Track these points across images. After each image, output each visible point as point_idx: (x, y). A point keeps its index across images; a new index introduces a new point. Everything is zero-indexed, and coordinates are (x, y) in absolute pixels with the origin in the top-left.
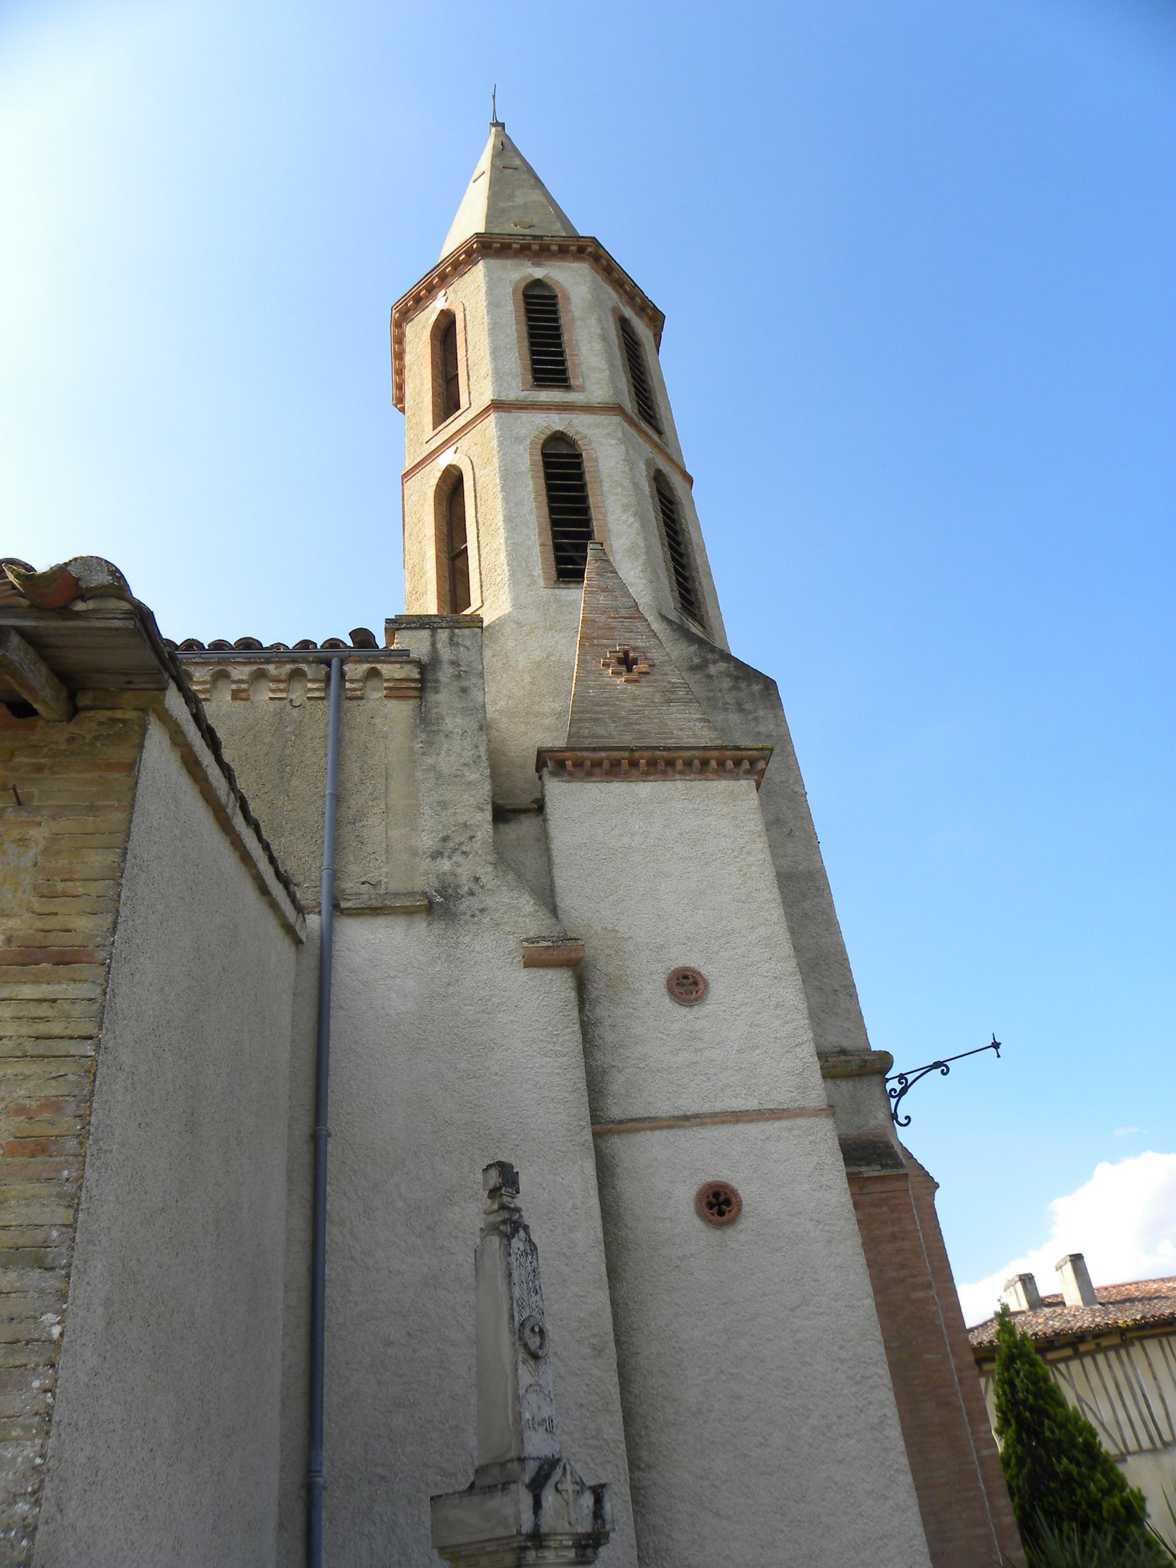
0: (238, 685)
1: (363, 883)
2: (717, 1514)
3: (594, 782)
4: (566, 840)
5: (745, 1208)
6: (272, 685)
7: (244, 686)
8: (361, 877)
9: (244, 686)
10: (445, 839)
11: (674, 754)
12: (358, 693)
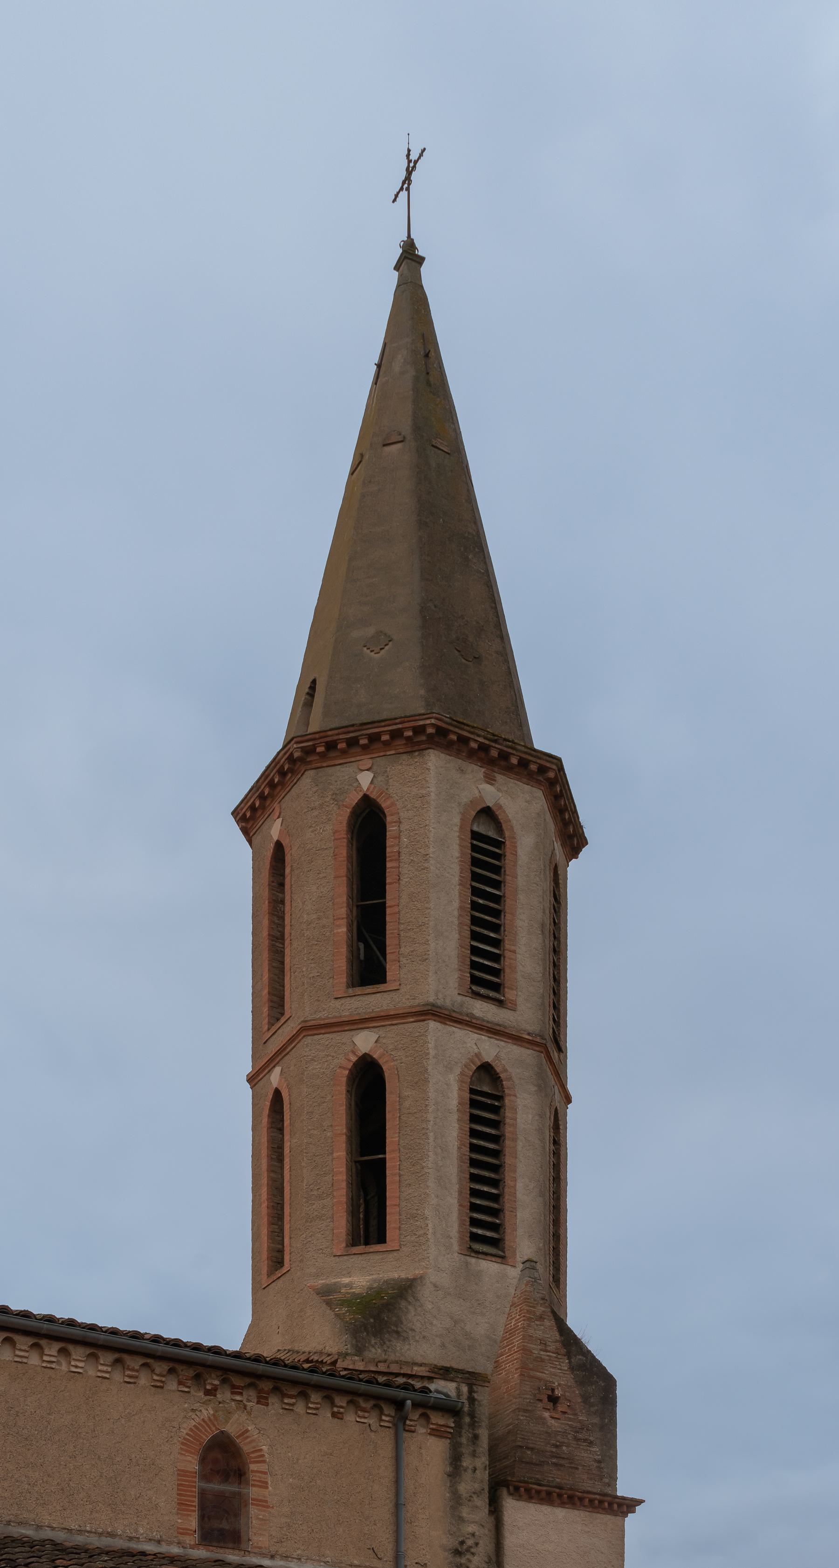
0: (339, 1409)
1: (416, 1563)
3: (533, 1503)
4: (513, 1540)
7: (342, 1410)
8: (415, 1559)
9: (342, 1410)
10: (462, 1543)
11: (585, 1495)
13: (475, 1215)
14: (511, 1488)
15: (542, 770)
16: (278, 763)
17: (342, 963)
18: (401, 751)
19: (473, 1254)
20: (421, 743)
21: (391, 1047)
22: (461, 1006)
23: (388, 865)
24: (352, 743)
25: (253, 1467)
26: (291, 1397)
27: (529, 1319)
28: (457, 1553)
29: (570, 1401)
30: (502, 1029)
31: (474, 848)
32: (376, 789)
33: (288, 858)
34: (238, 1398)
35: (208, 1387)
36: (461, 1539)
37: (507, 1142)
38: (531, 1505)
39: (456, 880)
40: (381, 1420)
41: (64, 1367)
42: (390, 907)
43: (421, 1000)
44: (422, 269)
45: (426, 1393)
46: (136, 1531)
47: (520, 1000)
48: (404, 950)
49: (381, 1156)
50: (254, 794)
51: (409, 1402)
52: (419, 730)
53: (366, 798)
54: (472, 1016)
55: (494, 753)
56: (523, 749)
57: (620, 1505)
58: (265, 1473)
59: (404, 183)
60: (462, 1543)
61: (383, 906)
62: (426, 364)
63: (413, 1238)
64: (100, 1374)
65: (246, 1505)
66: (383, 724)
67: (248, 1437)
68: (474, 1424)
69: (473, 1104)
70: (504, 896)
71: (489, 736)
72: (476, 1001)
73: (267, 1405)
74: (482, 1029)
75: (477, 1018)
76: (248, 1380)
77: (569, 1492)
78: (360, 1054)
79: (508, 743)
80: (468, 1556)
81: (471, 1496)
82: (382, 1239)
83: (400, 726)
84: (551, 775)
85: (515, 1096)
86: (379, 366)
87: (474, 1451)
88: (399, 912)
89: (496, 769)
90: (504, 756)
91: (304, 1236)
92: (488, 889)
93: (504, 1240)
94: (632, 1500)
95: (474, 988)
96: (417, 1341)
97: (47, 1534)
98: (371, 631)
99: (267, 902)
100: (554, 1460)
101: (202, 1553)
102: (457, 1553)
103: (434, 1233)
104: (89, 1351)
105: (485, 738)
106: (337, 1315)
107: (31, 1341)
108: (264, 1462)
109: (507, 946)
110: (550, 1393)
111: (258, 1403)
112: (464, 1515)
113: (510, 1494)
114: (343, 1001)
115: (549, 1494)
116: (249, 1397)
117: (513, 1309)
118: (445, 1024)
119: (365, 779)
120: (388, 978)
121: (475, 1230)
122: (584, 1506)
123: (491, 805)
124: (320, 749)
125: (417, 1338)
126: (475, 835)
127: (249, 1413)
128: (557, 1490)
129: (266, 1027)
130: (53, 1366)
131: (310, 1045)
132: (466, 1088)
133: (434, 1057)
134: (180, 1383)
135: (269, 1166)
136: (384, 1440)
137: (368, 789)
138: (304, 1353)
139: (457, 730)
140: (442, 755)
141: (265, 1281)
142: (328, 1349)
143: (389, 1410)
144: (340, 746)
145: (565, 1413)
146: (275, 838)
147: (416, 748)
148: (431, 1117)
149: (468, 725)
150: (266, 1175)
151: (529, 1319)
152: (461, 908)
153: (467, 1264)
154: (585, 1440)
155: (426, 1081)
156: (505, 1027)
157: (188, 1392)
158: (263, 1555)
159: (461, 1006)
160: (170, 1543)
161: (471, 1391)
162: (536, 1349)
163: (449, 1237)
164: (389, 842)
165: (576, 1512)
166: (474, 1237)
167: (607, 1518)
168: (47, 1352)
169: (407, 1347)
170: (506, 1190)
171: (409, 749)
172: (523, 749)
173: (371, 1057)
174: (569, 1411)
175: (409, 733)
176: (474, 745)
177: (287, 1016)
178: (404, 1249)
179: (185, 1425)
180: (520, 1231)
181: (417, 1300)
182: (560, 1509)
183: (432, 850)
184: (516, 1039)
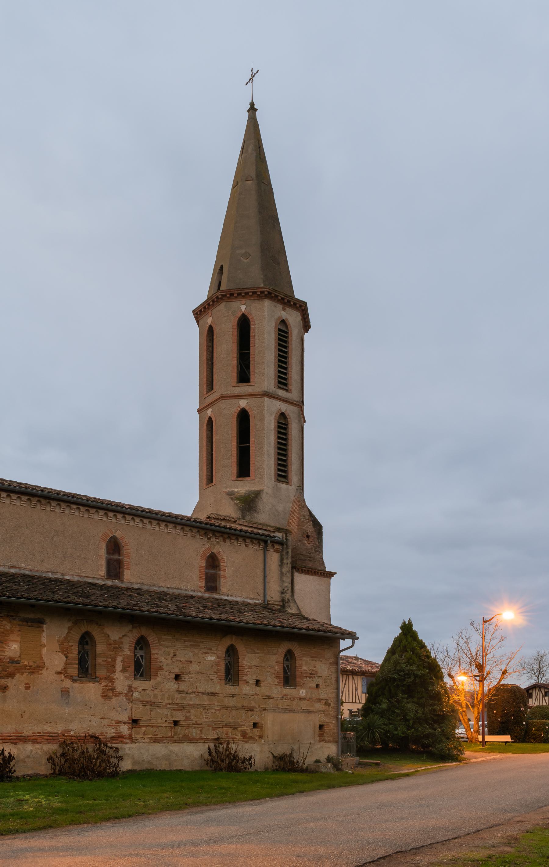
9: (248, 544)
10: (284, 589)
13: (279, 467)
14: (297, 569)
15: (301, 306)
16: (213, 297)
17: (235, 374)
18: (255, 298)
20: (262, 296)
21: (252, 406)
22: (275, 392)
23: (251, 340)
24: (239, 294)
25: (222, 564)
26: (233, 540)
27: (300, 508)
28: (282, 593)
29: (313, 537)
30: (288, 400)
31: (279, 334)
32: (247, 312)
33: (215, 333)
34: (217, 540)
35: (209, 537)
36: (283, 588)
37: (289, 441)
38: (302, 575)
39: (273, 346)
40: (260, 547)
41: (166, 531)
42: (252, 355)
43: (262, 390)
44: (256, 112)
45: (274, 538)
46: (187, 587)
47: (293, 389)
48: (257, 371)
49: (248, 445)
50: (202, 306)
51: (269, 541)
52: (262, 292)
53: (243, 314)
54: (278, 395)
55: (286, 301)
57: (329, 574)
59: (250, 80)
60: (284, 589)
61: (249, 353)
62: (259, 150)
63: (260, 476)
64: (177, 533)
65: (220, 577)
66: (250, 289)
67: (220, 554)
68: (287, 548)
69: (279, 427)
70: (288, 352)
71: (285, 295)
73: (226, 542)
74: (281, 400)
75: (280, 396)
76: (221, 534)
77: (315, 570)
78: (241, 408)
80: (286, 594)
82: (248, 475)
83: (256, 290)
84: (303, 308)
85: (292, 424)
86: (243, 149)
87: (287, 557)
88: (255, 357)
89: (286, 306)
90: (289, 302)
91: (222, 473)
93: (288, 476)
94: (333, 573)
95: (279, 385)
96: (261, 513)
97: (162, 589)
98: (243, 251)
99: (206, 346)
100: (309, 559)
101: (207, 595)
102: (282, 593)
103: (267, 474)
104: (174, 525)
105: (283, 295)
106: (236, 504)
107: (157, 522)
108: (225, 562)
109: (289, 370)
110: (307, 534)
112: (284, 580)
113: (296, 571)
114: (235, 388)
115: (308, 571)
116: (220, 540)
117: (294, 503)
119: (243, 308)
120: (251, 381)
121: (279, 473)
122: (319, 575)
123: (284, 319)
124: (228, 296)
125: (261, 512)
126: (280, 330)
127: (221, 546)
128: (311, 570)
129: (205, 393)
130: (163, 530)
131: (224, 403)
132: (277, 421)
133: (267, 411)
134: (200, 535)
135: (207, 444)
136: (260, 554)
137: (244, 311)
138: (222, 516)
139: (275, 293)
140: (269, 301)
141: (205, 487)
142: (232, 516)
143: (262, 544)
144: (235, 295)
145: (311, 541)
146: (209, 323)
147: (261, 298)
148: (265, 432)
149: (278, 291)
150: (205, 447)
151: (300, 508)
152: (275, 356)
153: (277, 485)
154: (318, 551)
155: (264, 419)
156: (288, 399)
157: (202, 538)
158: (225, 595)
159: (275, 392)
160: (198, 592)
161: (286, 536)
162: (302, 518)
163: (271, 476)
164: (251, 331)
165: (316, 577)
166: (279, 475)
167: (325, 579)
168: (161, 526)
169: (258, 515)
170: (289, 458)
171: (258, 298)
173: (245, 409)
174: (313, 541)
175: (259, 293)
176: (280, 298)
177: (214, 390)
178: (256, 479)
179: (201, 550)
180: (293, 473)
181: (261, 498)
183: (266, 335)
184: (292, 403)
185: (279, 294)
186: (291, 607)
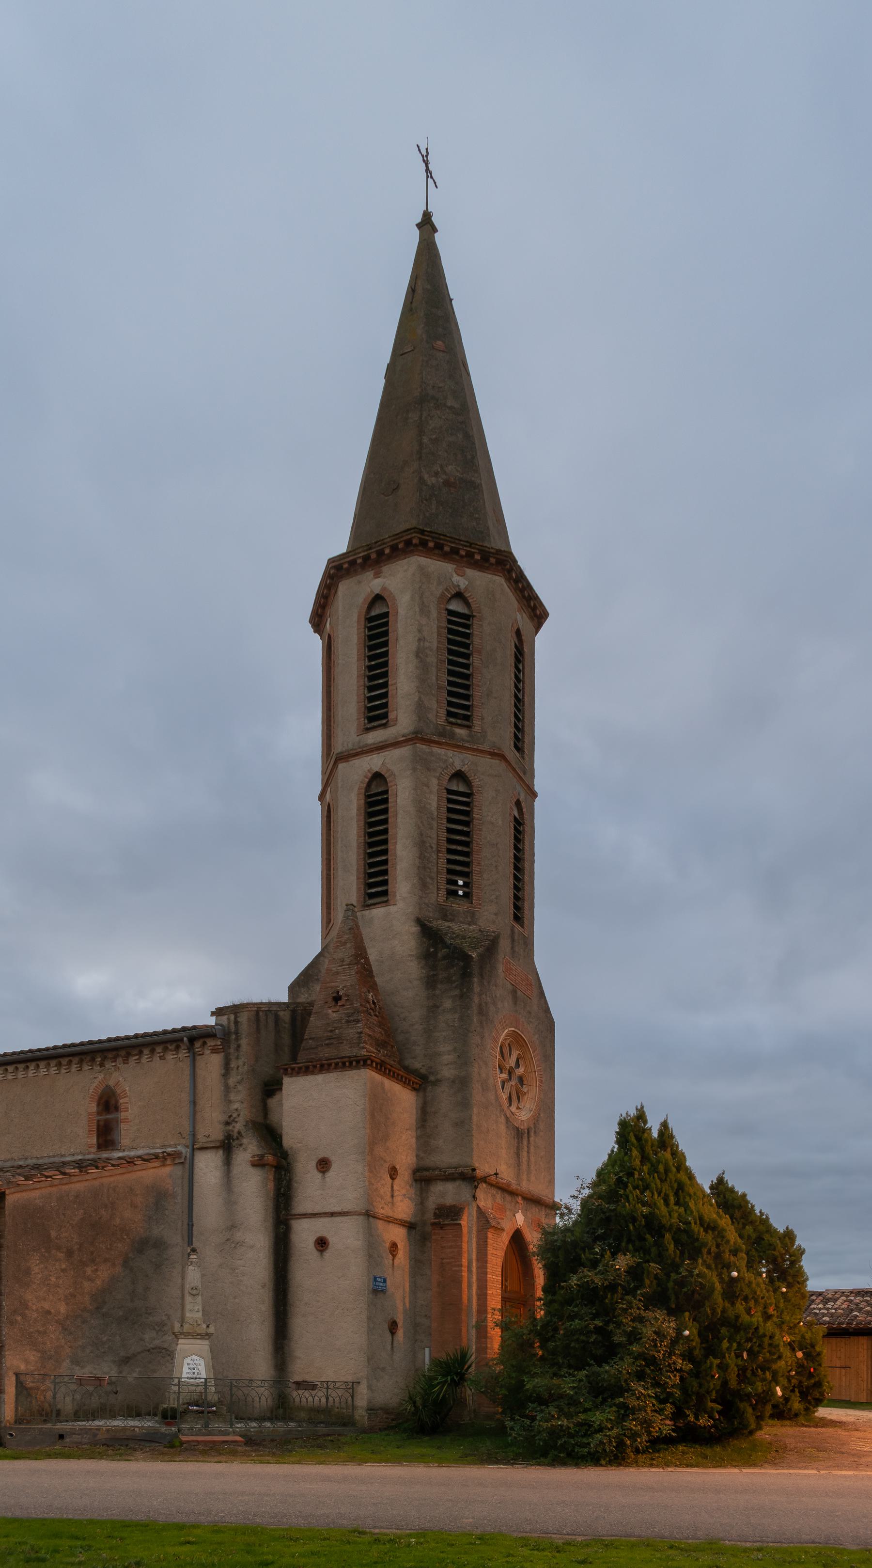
2: (307, 1332)
5: (330, 1246)
6: (171, 1053)
10: (230, 1116)
12: (201, 1052)
19: (366, 908)
28: (227, 1123)
36: (229, 1115)
38: (299, 1078)
54: (367, 745)
56: (389, 539)
58: (127, 1103)
72: (369, 734)
74: (372, 751)
79: (378, 543)
80: (234, 1124)
81: (236, 1086)
87: (238, 1055)
92: (378, 651)
108: (127, 1097)
111: (124, 1063)
112: (232, 1098)
118: (348, 761)
165: (331, 1074)
172: (389, 539)
182: (320, 1075)
185: (355, 555)
186: (244, 1146)
